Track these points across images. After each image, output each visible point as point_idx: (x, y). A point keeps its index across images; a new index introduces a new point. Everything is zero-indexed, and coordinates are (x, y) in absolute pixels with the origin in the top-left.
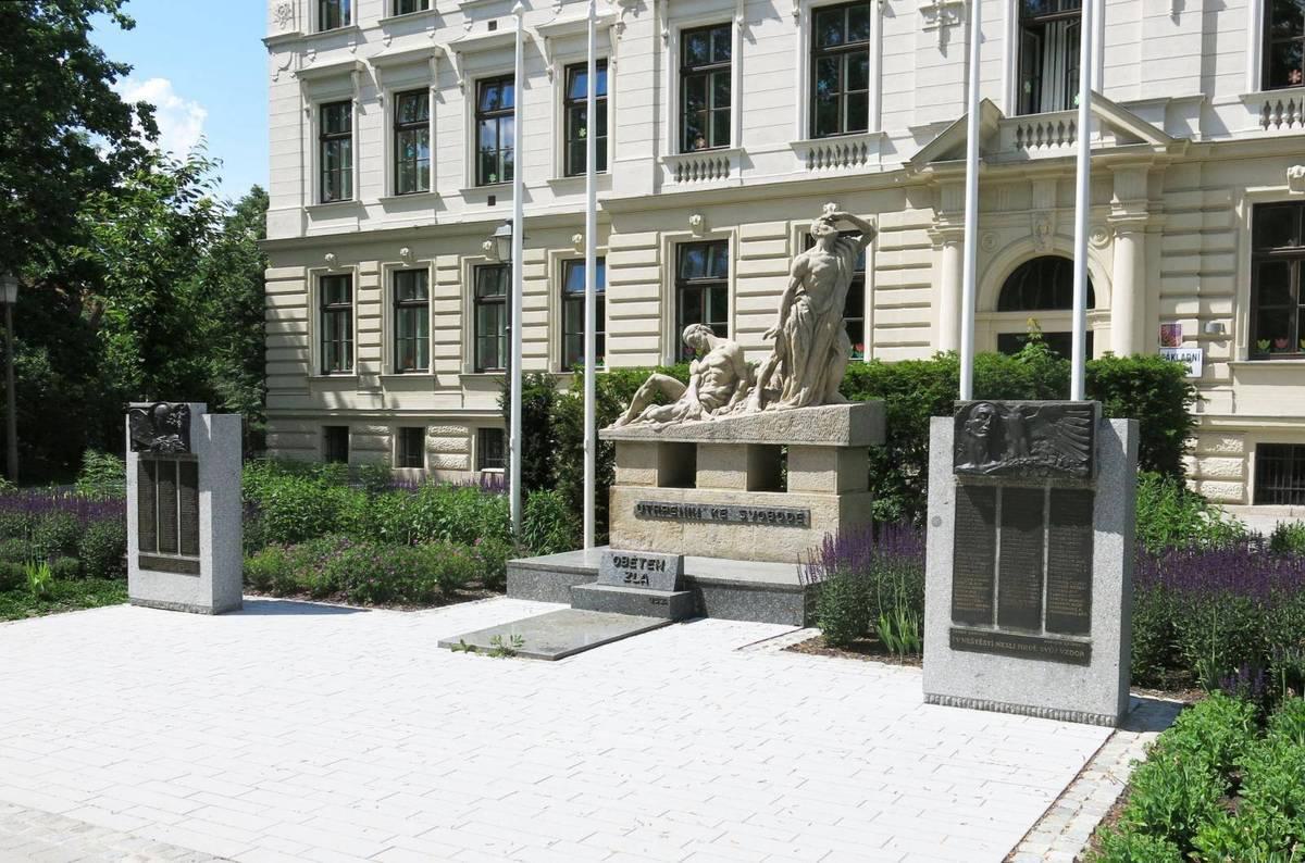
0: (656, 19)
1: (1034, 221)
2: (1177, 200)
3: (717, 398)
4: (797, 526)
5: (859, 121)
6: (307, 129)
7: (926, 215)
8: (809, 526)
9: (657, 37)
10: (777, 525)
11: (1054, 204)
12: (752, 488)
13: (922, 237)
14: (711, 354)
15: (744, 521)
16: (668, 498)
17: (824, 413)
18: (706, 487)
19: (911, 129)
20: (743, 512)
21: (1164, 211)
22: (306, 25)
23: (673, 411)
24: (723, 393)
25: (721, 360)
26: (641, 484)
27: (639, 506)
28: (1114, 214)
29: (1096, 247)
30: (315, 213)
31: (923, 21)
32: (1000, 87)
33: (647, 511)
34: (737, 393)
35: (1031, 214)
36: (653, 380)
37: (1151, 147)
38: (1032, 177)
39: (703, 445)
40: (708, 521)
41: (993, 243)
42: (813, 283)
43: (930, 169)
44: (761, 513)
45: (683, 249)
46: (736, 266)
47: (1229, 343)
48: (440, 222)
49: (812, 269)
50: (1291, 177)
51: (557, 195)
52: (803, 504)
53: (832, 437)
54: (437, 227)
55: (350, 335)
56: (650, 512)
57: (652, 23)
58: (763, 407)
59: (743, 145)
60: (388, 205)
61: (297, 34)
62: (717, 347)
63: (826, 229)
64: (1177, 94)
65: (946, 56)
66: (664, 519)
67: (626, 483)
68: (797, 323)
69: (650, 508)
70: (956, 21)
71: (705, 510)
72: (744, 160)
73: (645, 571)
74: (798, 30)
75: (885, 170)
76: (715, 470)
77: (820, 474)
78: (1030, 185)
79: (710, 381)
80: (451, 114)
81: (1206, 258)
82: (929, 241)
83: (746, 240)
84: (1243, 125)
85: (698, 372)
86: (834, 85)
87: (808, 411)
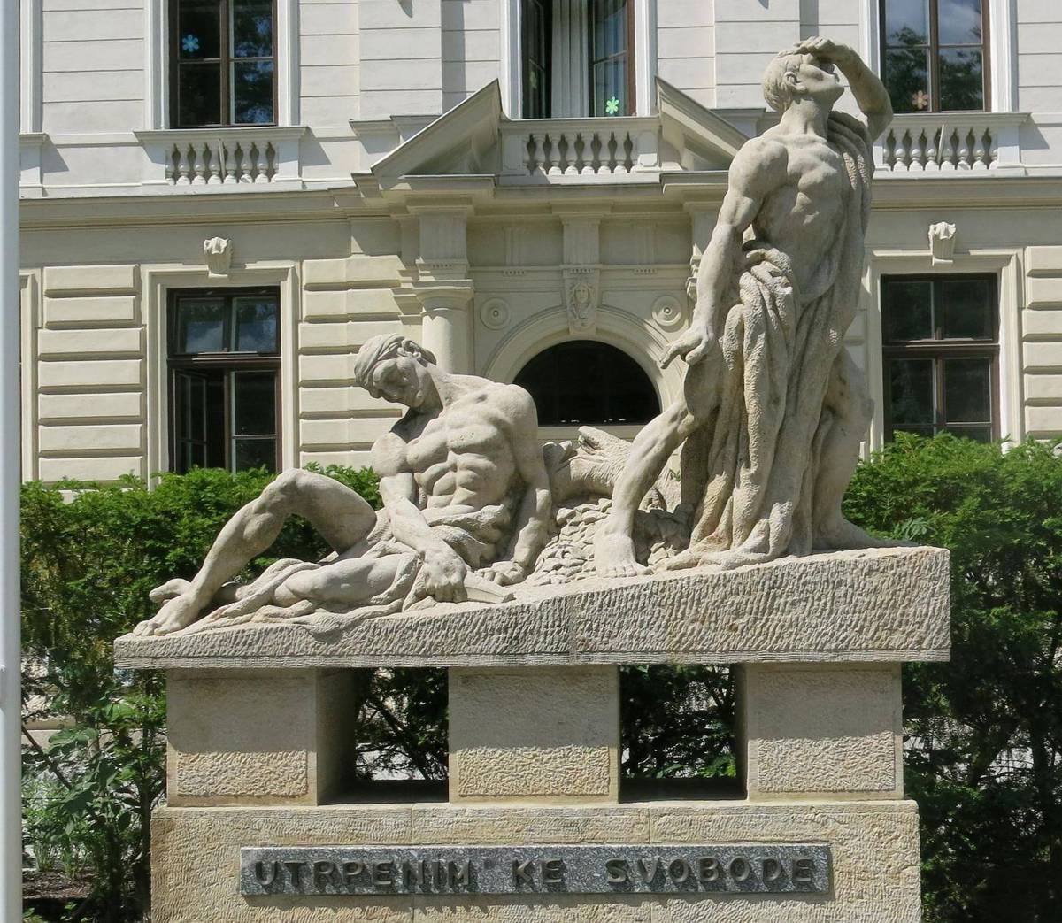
1: (567, 284)
3: (484, 539)
4: (789, 895)
7: (388, 266)
8: (827, 895)
10: (729, 896)
11: (597, 258)
12: (634, 786)
13: (383, 301)
14: (446, 416)
15: (622, 892)
16: (359, 838)
17: (871, 571)
18: (484, 797)
19: (353, 124)
20: (616, 866)
23: (373, 574)
24: (496, 525)
25: (487, 432)
26: (259, 799)
27: (259, 869)
29: (663, 327)
34: (532, 523)
35: (561, 272)
38: (563, 214)
39: (471, 676)
40: (502, 899)
41: (501, 317)
42: (801, 216)
43: (406, 186)
44: (678, 868)
49: (798, 176)
50: (936, 237)
52: (809, 831)
53: (897, 639)
56: (297, 881)
58: (642, 557)
62: (461, 398)
63: (819, 78)
65: (411, 16)
66: (350, 899)
67: (207, 798)
68: (763, 324)
69: (297, 870)
71: (489, 865)
76: (513, 743)
77: (850, 743)
78: (559, 227)
79: (450, 490)
82: (393, 308)
83: (54, 294)
85: (406, 467)
86: (210, 45)
87: (820, 569)
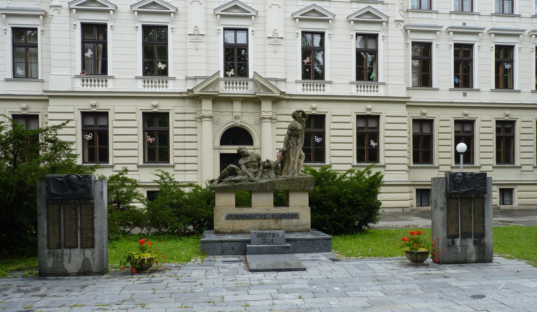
27: (227, 216)
33: (230, 217)
36: (230, 167)
73: (271, 238)
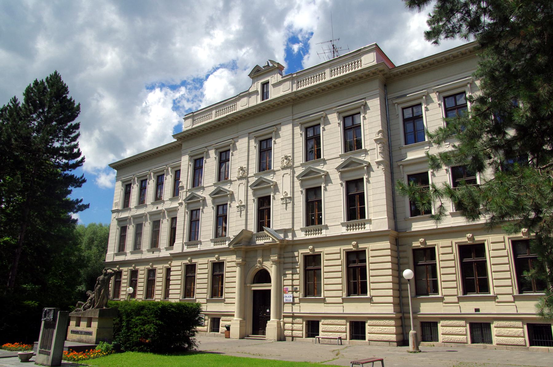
0: (185, 208)
2: (286, 255)
5: (363, 215)
6: (117, 233)
9: (185, 212)
21: (284, 258)
22: (120, 207)
28: (271, 258)
30: (117, 255)
31: (281, 202)
32: (252, 227)
37: (276, 242)
45: (349, 254)
46: (369, 259)
47: (299, 292)
48: (142, 258)
51: (452, 217)
54: (437, 229)
55: (222, 284)
57: (184, 209)
59: (201, 240)
60: (149, 251)
61: (118, 209)
64: (287, 228)
70: (290, 202)
72: (200, 243)
74: (342, 188)
75: (327, 236)
80: (147, 229)
81: (293, 270)
84: (301, 236)
